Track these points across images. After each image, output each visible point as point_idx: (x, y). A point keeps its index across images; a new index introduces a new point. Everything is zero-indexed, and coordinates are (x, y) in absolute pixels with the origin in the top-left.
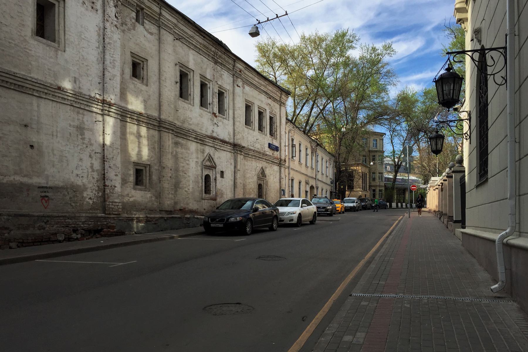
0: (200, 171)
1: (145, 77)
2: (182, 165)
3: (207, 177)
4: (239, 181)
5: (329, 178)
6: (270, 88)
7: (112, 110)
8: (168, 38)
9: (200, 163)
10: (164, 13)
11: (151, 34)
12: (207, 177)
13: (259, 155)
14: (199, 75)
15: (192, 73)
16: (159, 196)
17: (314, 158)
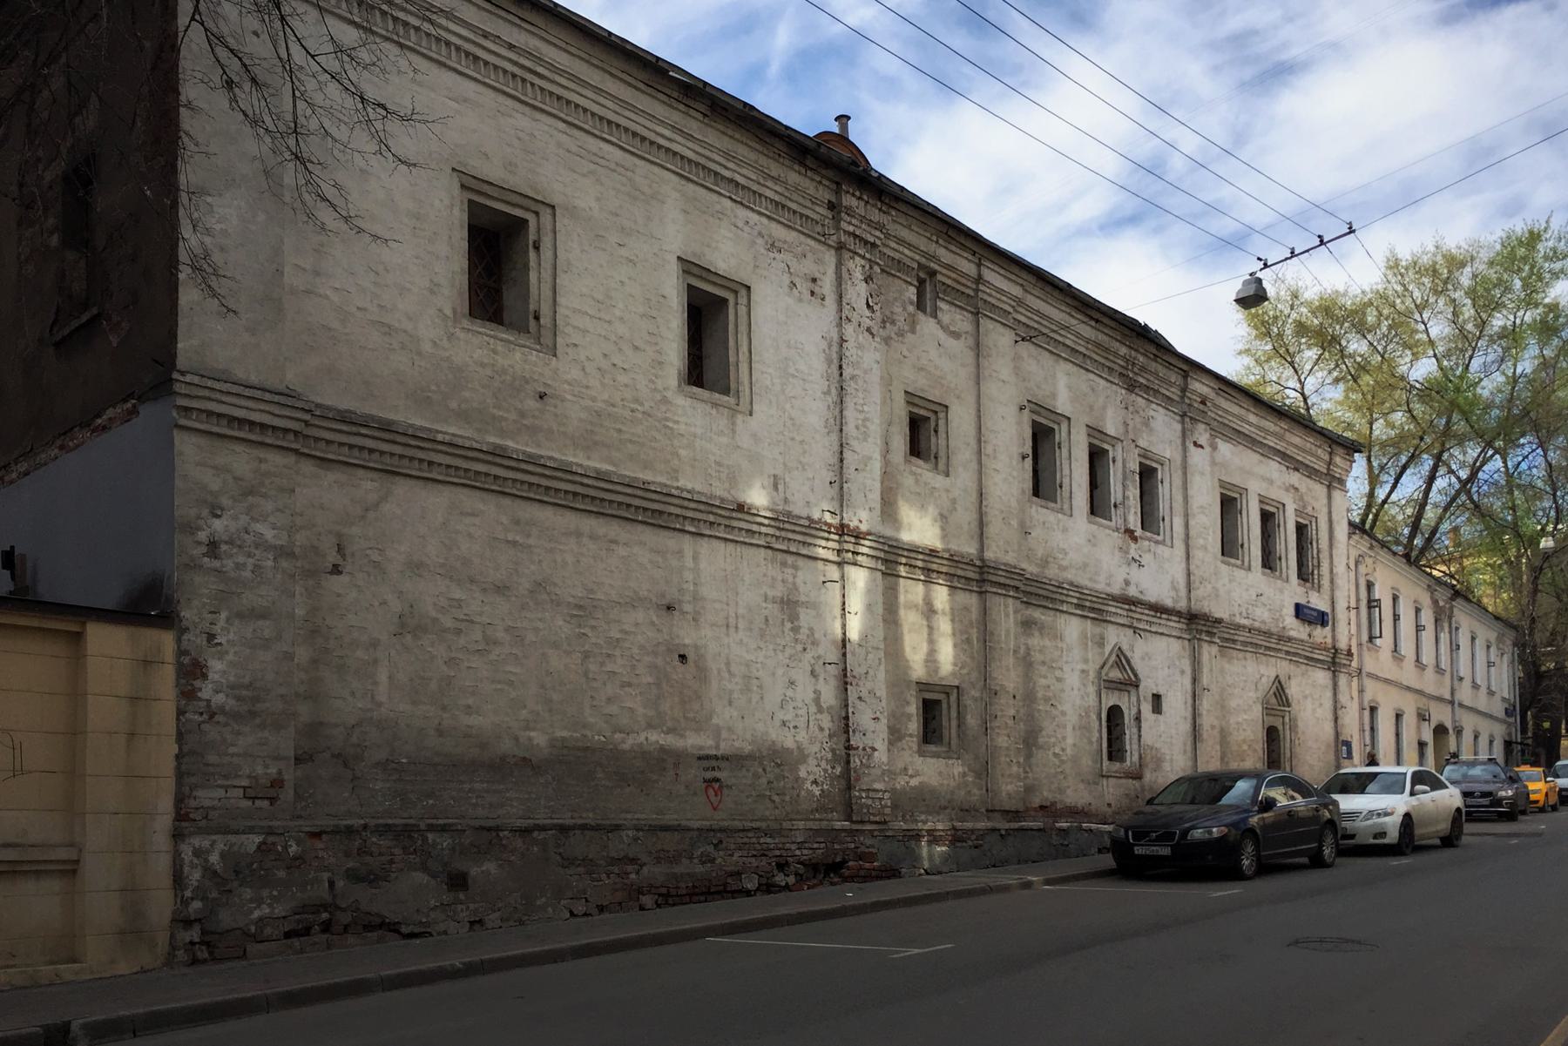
1: (942, 454)
2: (1043, 682)
3: (1114, 714)
5: (1497, 698)
6: (1296, 440)
8: (1000, 338)
9: (1092, 675)
10: (988, 275)
12: (1114, 714)
14: (1084, 430)
15: (743, 300)
16: (984, 770)
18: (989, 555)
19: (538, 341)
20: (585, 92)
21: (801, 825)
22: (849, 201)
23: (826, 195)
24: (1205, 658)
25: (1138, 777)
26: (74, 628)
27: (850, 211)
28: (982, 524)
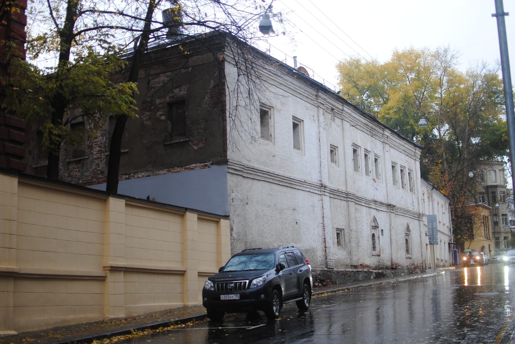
0: (370, 231)
1: (337, 161)
2: (360, 227)
3: (373, 235)
4: (393, 238)
5: (446, 226)
6: (407, 146)
7: (326, 191)
8: (347, 125)
9: (369, 224)
10: (345, 109)
11: (338, 126)
12: (373, 235)
13: (406, 212)
14: (364, 150)
15: (302, 124)
16: (350, 253)
17: (431, 203)
18: (348, 190)
19: (271, 141)
20: (264, 70)
21: (319, 269)
22: (320, 94)
23: (315, 93)
24: (392, 218)
25: (379, 256)
26: (218, 220)
27: (320, 97)
28: (346, 181)
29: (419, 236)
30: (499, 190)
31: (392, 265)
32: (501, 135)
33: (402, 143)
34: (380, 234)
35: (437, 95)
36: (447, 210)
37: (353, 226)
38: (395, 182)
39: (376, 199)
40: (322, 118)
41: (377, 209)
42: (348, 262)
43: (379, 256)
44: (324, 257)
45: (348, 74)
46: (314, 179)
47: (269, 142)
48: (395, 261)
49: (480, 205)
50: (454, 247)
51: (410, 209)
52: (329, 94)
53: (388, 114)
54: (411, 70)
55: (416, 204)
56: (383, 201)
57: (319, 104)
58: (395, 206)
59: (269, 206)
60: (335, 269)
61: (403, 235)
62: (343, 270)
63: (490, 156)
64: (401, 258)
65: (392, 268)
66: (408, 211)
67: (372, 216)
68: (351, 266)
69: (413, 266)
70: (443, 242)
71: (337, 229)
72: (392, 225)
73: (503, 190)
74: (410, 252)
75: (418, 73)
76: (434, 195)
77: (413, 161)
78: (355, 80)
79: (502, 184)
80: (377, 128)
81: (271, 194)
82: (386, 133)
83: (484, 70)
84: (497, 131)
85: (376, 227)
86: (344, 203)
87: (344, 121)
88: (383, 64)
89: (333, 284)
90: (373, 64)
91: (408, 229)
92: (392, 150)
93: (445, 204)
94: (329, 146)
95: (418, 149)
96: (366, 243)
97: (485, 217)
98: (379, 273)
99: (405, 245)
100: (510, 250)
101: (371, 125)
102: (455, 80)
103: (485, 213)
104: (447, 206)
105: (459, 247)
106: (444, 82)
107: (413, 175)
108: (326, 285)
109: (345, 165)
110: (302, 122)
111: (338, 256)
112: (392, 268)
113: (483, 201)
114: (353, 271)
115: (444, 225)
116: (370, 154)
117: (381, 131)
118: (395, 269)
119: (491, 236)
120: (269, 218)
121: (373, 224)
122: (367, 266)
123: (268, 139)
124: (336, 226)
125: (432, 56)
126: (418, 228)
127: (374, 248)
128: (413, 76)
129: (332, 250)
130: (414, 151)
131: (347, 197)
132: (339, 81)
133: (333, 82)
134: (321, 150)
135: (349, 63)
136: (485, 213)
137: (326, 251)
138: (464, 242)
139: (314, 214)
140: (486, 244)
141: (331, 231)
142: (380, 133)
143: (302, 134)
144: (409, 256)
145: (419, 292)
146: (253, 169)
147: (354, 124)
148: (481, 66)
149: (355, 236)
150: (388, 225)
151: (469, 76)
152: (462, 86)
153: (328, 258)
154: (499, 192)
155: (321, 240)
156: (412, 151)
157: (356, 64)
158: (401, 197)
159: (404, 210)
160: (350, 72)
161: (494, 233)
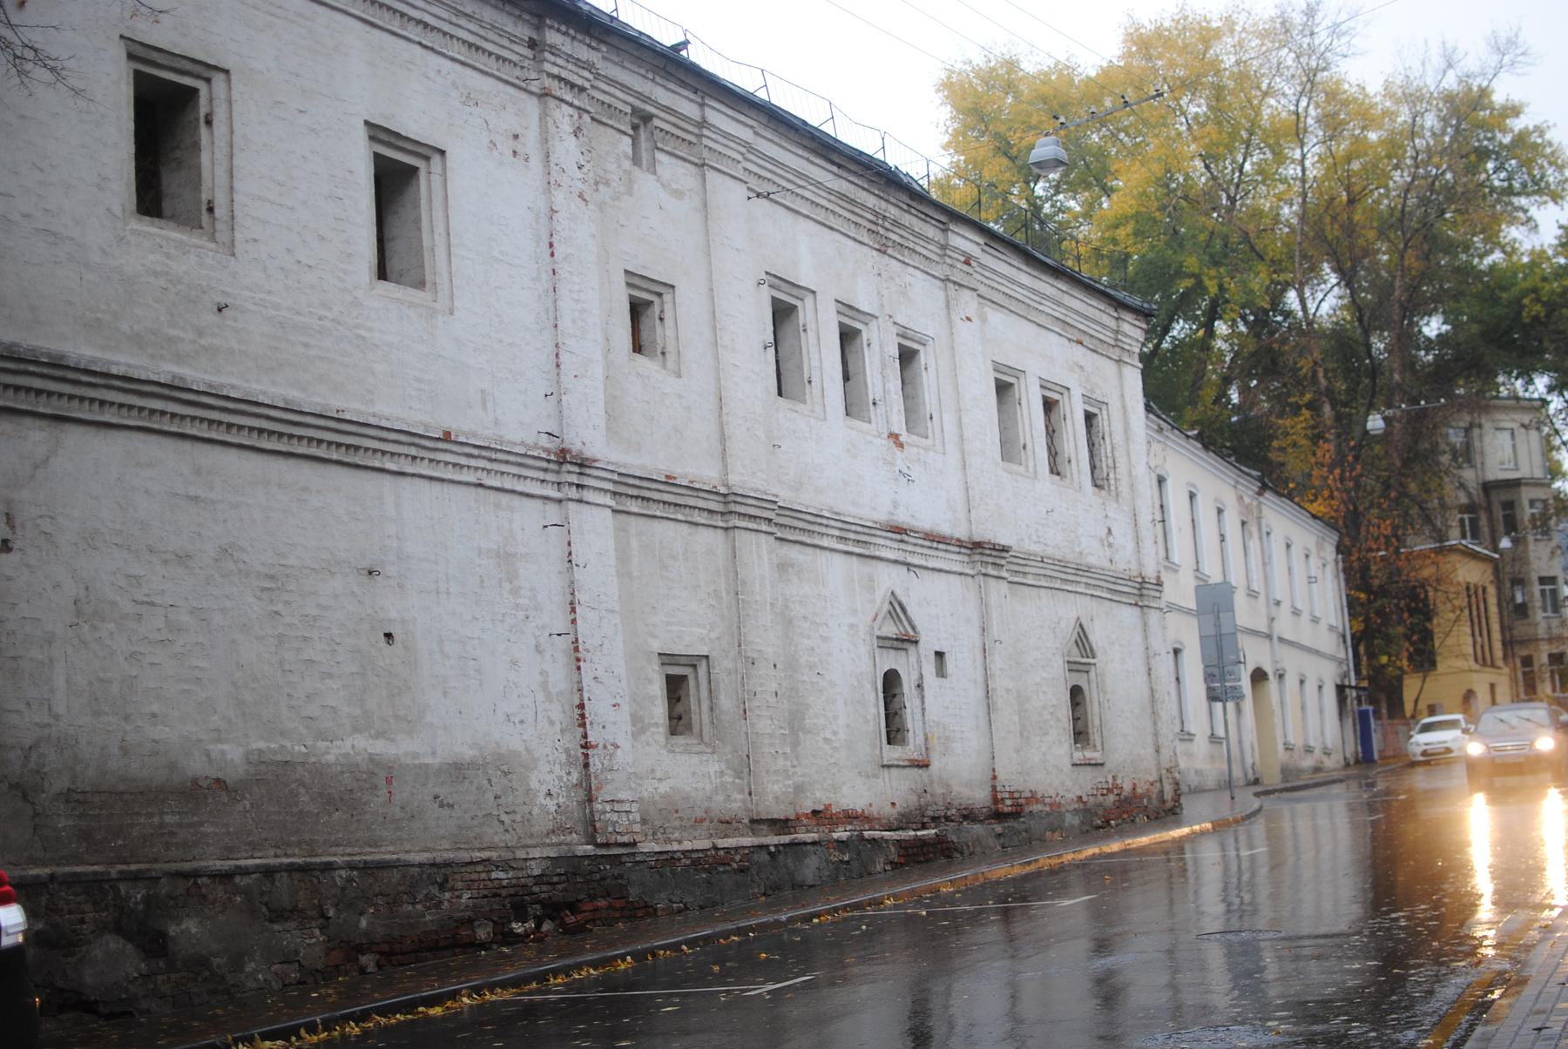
1: (670, 348)
3: (891, 681)
4: (1000, 683)
5: (1323, 626)
9: (862, 628)
10: (714, 117)
11: (678, 194)
12: (891, 681)
13: (1068, 574)
14: (833, 307)
16: (745, 766)
17: (1254, 545)
18: (734, 479)
19: (213, 239)
21: (536, 853)
22: (552, 37)
23: (524, 32)
24: (994, 599)
25: (924, 765)
27: (554, 51)
28: (723, 438)
29: (1143, 669)
30: (1527, 494)
31: (996, 800)
32: (1519, 300)
33: (1049, 290)
34: (929, 668)
35: (1292, 171)
36: (1330, 569)
37: (765, 639)
38: (1010, 448)
39: (902, 518)
40: (567, 150)
41: (908, 565)
42: (736, 804)
43: (924, 765)
44: (581, 794)
45: (975, 110)
46: (518, 421)
47: (203, 242)
48: (1011, 777)
49: (1452, 549)
50: (1359, 698)
51: (1096, 557)
52: (611, 39)
53: (1115, 241)
54: (1191, 85)
55: (1123, 537)
56: (945, 529)
57: (548, 82)
58: (1005, 549)
59: (183, 558)
60: (648, 846)
61: (1058, 667)
62: (706, 844)
63: (1488, 376)
64: (1047, 768)
65: (998, 816)
66: (1082, 570)
67: (881, 595)
68: (753, 821)
69: (1112, 798)
70: (1311, 686)
71: (667, 658)
72: (995, 630)
73: (1539, 493)
74: (1095, 737)
75: (1219, 92)
76: (1266, 511)
77: (1109, 368)
78: (1002, 129)
79: (1538, 473)
80: (907, 219)
81: (196, 499)
82: (956, 241)
83: (1451, 74)
84: (1504, 289)
85: (905, 642)
86: (713, 539)
87: (710, 174)
88: (1093, 73)
89: (631, 917)
90: (1065, 73)
91: (1082, 639)
92: (996, 317)
93: (1320, 547)
94: (621, 279)
95: (1128, 317)
96: (846, 709)
97: (1473, 593)
98: (922, 843)
99: (1065, 712)
100: (423, 773)
101: (871, 201)
102: (1341, 111)
103: (1469, 573)
104: (1330, 552)
105: (1383, 697)
106: (1310, 121)
107: (1111, 422)
108: (580, 929)
109: (717, 370)
110: (436, 159)
111: (663, 784)
112: (998, 816)
113: (1475, 535)
114: (761, 847)
115: (1315, 620)
116: (873, 324)
117: (931, 232)
118: (1016, 814)
119: (1499, 653)
120: (185, 618)
121: (890, 630)
122: (850, 817)
123: (190, 222)
124: (657, 646)
125: (1264, 35)
126: (1138, 638)
127: (894, 731)
128: (1197, 107)
129: (623, 757)
130: (1113, 324)
131: (728, 509)
132: (947, 138)
133: (922, 146)
134: (563, 290)
135: (978, 73)
136: (1469, 573)
137: (586, 766)
138: (1400, 680)
139: (515, 592)
140: (1480, 682)
141: (621, 670)
142: (928, 240)
143: (438, 215)
144: (1089, 754)
145: (1144, 907)
146: (57, 367)
147: (765, 188)
148: (1437, 61)
149: (774, 686)
150: (974, 632)
151: (1398, 102)
152: (1373, 136)
153: (604, 794)
154: (1526, 503)
155: (559, 713)
156: (1104, 326)
157: (1004, 77)
158: (1036, 510)
159: (1062, 564)
160: (992, 109)
161: (1508, 644)
